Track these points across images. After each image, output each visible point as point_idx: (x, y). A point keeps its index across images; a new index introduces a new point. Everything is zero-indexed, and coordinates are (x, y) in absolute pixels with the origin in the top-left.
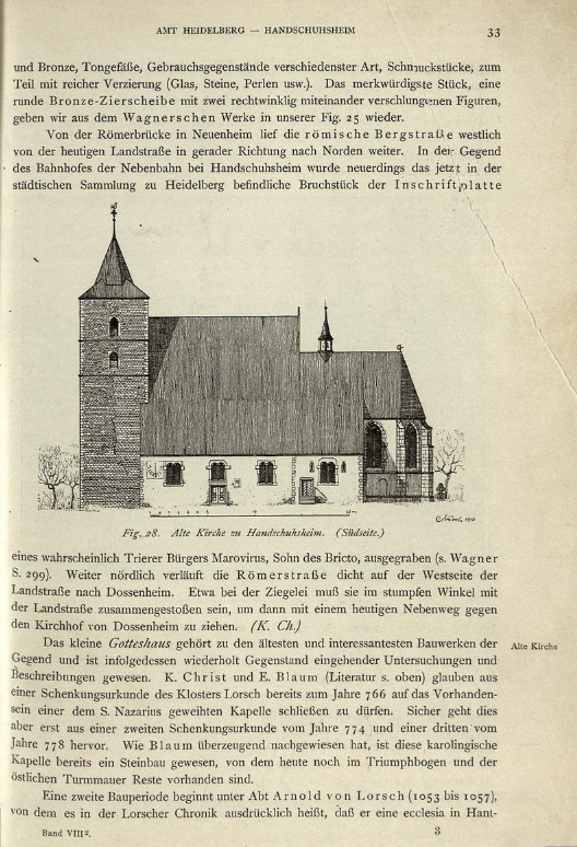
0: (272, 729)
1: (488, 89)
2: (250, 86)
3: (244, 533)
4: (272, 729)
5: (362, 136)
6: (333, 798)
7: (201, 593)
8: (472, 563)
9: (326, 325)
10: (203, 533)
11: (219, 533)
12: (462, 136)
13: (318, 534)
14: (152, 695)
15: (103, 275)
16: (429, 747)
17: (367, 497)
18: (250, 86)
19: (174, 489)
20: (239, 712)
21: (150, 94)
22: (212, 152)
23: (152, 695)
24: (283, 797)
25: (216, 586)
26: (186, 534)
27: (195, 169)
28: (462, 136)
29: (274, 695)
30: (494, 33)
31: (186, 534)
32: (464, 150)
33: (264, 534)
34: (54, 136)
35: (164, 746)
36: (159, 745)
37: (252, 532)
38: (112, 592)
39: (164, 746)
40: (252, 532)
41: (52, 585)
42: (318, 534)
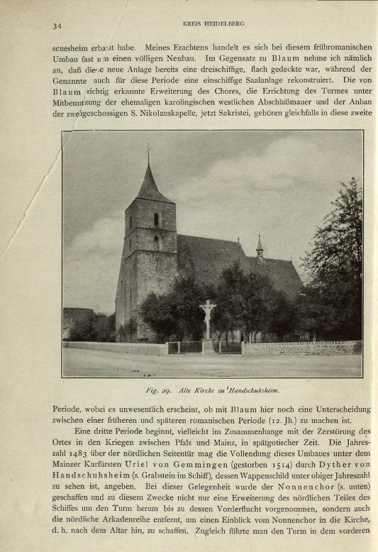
0: (140, 432)
2: (155, 81)
4: (140, 432)
5: (341, 466)
6: (359, 466)
7: (158, 92)
8: (152, 62)
9: (260, 242)
10: (199, 391)
11: (210, 391)
15: (143, 189)
18: (155, 81)
19: (54, 330)
20: (90, 465)
22: (217, 81)
24: (108, 520)
25: (144, 493)
27: (277, 48)
29: (160, 70)
35: (62, 93)
36: (278, 58)
38: (332, 442)
39: (62, 93)
40: (232, 390)
41: (327, 437)
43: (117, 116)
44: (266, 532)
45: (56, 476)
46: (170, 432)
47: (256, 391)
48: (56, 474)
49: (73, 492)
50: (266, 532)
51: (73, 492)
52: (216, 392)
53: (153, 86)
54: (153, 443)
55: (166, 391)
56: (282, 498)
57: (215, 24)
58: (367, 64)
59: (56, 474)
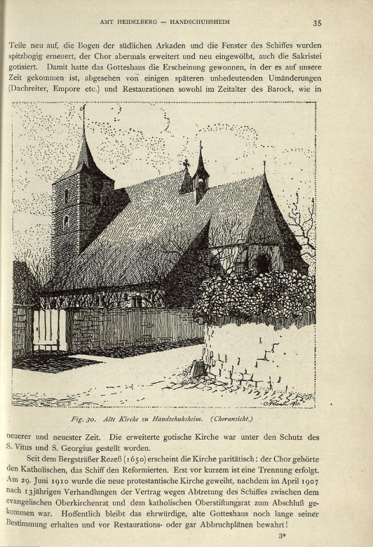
1: (150, 82)
3: (151, 419)
10: (124, 419)
11: (135, 420)
12: (78, 89)
13: (199, 419)
14: (90, 67)
16: (150, 504)
17: (313, 319)
21: (216, 498)
23: (90, 67)
26: (113, 419)
28: (78, 89)
30: (318, 23)
31: (113, 419)
32: (213, 513)
33: (163, 419)
34: (69, 493)
37: (156, 419)
38: (113, 437)
40: (156, 419)
42: (199, 419)
43: (202, 148)
44: (77, 525)
45: (65, 515)
46: (247, 503)
47: (179, 420)
48: (65, 512)
49: (27, 508)
50: (77, 525)
51: (27, 508)
52: (221, 439)
53: (270, 84)
54: (175, 504)
55: (91, 420)
56: (133, 514)
57: (129, 22)
58: (14, 51)
59: (65, 512)
